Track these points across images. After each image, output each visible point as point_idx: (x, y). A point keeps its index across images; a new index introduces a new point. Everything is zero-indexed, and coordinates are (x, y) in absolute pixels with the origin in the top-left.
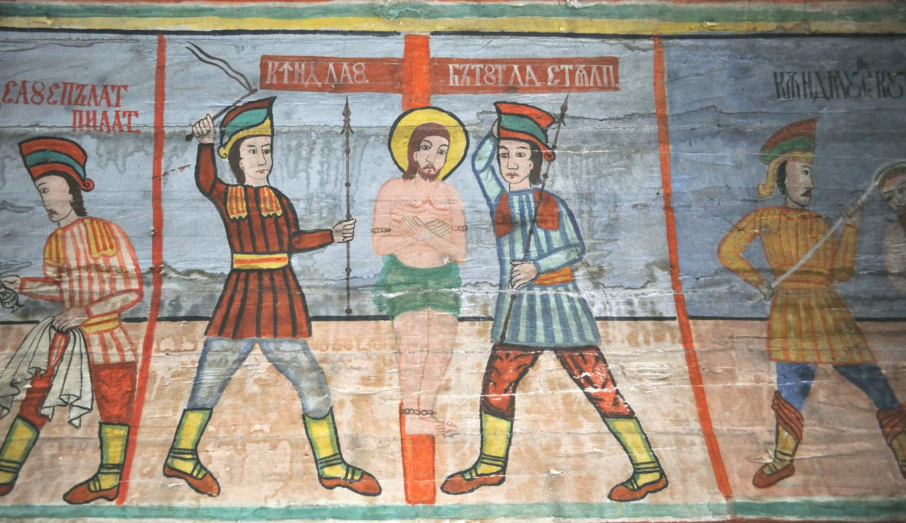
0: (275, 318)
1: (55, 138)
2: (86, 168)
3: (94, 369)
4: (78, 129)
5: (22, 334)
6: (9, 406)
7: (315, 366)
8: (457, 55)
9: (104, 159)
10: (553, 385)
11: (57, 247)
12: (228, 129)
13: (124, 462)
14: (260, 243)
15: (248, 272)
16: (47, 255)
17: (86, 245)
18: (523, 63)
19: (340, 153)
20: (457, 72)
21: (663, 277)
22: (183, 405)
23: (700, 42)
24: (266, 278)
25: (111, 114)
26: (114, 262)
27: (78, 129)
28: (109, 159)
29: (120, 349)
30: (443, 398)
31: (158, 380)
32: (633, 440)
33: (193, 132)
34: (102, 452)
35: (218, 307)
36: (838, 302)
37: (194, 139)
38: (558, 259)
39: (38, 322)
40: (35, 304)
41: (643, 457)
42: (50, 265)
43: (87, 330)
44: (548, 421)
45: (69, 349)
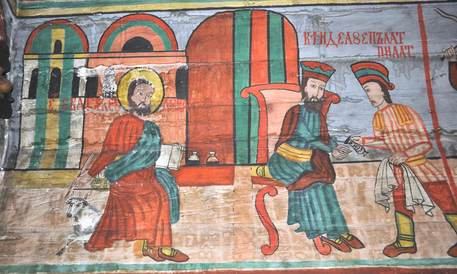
1: (370, 62)
2: (389, 77)
3: (427, 186)
4: (381, 57)
6: (388, 206)
9: (398, 72)
11: (380, 120)
16: (375, 125)
17: (396, 119)
26: (412, 127)
27: (381, 57)
28: (400, 72)
29: (434, 174)
34: (454, 229)
39: (381, 161)
40: (375, 151)
43: (410, 164)
45: (405, 174)
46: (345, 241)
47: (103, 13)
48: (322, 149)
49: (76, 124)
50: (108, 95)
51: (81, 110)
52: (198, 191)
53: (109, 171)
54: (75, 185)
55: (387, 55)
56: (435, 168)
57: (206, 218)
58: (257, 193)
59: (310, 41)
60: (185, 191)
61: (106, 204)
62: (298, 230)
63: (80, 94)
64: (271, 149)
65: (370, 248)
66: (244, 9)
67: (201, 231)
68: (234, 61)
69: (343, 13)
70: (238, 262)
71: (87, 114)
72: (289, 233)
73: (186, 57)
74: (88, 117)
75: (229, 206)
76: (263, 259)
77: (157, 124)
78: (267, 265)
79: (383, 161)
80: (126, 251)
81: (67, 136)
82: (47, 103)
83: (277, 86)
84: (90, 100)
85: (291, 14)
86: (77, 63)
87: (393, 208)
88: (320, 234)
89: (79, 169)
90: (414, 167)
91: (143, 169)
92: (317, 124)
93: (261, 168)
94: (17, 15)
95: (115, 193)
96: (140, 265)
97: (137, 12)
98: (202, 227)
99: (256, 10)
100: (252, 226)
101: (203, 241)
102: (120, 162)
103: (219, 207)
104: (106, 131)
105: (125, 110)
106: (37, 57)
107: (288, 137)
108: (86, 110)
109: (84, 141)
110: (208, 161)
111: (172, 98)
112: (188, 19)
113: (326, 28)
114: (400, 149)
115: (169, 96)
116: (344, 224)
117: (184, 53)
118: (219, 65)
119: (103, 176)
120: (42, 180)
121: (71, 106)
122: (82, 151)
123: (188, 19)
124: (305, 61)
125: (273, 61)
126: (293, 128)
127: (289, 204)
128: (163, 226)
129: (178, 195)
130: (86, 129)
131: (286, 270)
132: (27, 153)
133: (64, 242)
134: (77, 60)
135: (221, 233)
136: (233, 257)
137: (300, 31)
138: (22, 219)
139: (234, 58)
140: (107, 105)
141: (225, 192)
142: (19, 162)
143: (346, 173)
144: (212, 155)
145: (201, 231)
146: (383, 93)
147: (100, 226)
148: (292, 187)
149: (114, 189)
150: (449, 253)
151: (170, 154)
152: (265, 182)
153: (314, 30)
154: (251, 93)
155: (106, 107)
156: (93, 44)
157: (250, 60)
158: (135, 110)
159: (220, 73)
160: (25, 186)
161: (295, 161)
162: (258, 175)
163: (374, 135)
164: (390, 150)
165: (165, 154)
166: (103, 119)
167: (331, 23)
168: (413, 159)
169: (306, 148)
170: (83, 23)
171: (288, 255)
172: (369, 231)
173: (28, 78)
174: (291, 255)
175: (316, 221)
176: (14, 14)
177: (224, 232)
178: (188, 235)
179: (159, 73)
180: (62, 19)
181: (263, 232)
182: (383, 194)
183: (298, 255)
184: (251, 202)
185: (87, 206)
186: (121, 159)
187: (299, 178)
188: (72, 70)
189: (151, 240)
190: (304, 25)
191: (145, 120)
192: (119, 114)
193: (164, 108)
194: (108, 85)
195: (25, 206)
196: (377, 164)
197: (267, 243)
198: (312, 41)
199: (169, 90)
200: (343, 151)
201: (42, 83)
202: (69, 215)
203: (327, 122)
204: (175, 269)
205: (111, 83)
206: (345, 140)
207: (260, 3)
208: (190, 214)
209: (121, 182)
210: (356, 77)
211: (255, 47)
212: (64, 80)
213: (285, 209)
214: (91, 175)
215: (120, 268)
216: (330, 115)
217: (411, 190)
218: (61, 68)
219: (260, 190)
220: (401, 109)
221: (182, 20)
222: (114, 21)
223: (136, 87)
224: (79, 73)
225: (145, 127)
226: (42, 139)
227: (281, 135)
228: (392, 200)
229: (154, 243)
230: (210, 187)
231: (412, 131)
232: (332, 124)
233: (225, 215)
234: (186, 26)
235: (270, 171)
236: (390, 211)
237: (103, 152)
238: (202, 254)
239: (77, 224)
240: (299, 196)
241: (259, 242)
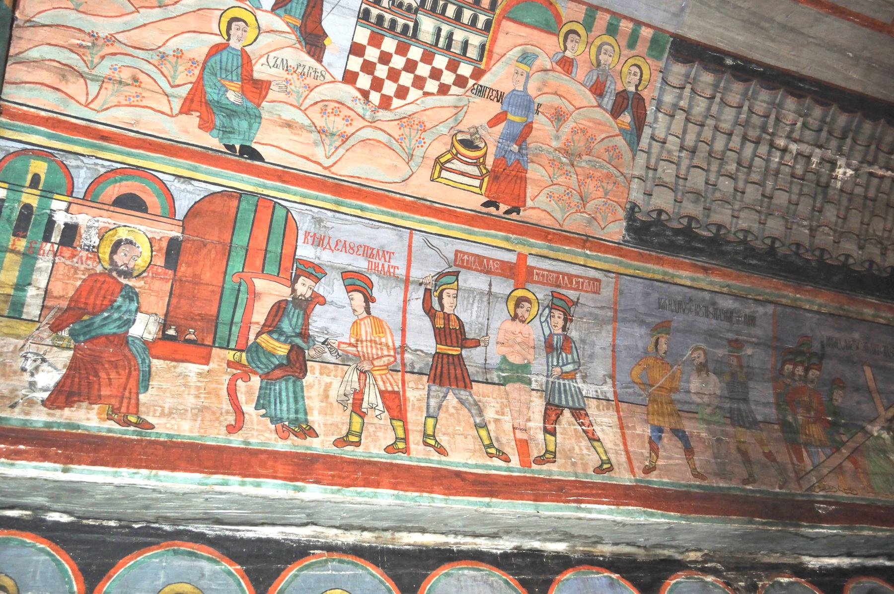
0: (456, 378)
3: (381, 392)
7: (476, 403)
8: (538, 266)
10: (570, 424)
12: (438, 283)
14: (449, 341)
15: (443, 354)
18: (564, 274)
19: (486, 303)
20: (537, 274)
21: (609, 381)
22: (425, 415)
23: (633, 279)
24: (451, 358)
26: (383, 340)
29: (391, 385)
30: (529, 424)
32: (600, 450)
35: (431, 369)
36: (672, 402)
38: (569, 368)
40: (347, 356)
41: (604, 458)
43: (374, 373)
44: (569, 439)
46: (303, 430)
47: (97, 158)
51: (51, 257)
53: (74, 329)
62: (263, 416)
63: (53, 240)
64: (252, 337)
66: (252, 194)
68: (231, 242)
77: (137, 290)
78: (230, 441)
82: (9, 241)
83: (269, 277)
84: (64, 248)
86: (55, 205)
87: (350, 408)
89: (38, 322)
91: (115, 334)
92: (300, 321)
93: (239, 353)
96: (103, 428)
100: (220, 406)
101: (171, 413)
106: (6, 186)
108: (57, 258)
117: (181, 223)
126: (277, 320)
129: (149, 367)
133: (17, 396)
139: (232, 240)
140: (84, 259)
143: (317, 371)
147: (59, 387)
148: (265, 377)
158: (116, 270)
166: (76, 273)
169: (285, 342)
170: (71, 162)
172: (325, 425)
174: (253, 435)
175: (281, 410)
177: (192, 409)
182: (345, 395)
184: (223, 384)
186: (90, 319)
187: (273, 370)
188: (48, 211)
189: (117, 406)
190: (306, 225)
196: (346, 368)
197: (233, 423)
198: (310, 241)
212: (36, 220)
227: (264, 325)
228: (351, 401)
229: (119, 409)
232: (313, 324)
234: (189, 196)
237: (69, 308)
239: (32, 379)
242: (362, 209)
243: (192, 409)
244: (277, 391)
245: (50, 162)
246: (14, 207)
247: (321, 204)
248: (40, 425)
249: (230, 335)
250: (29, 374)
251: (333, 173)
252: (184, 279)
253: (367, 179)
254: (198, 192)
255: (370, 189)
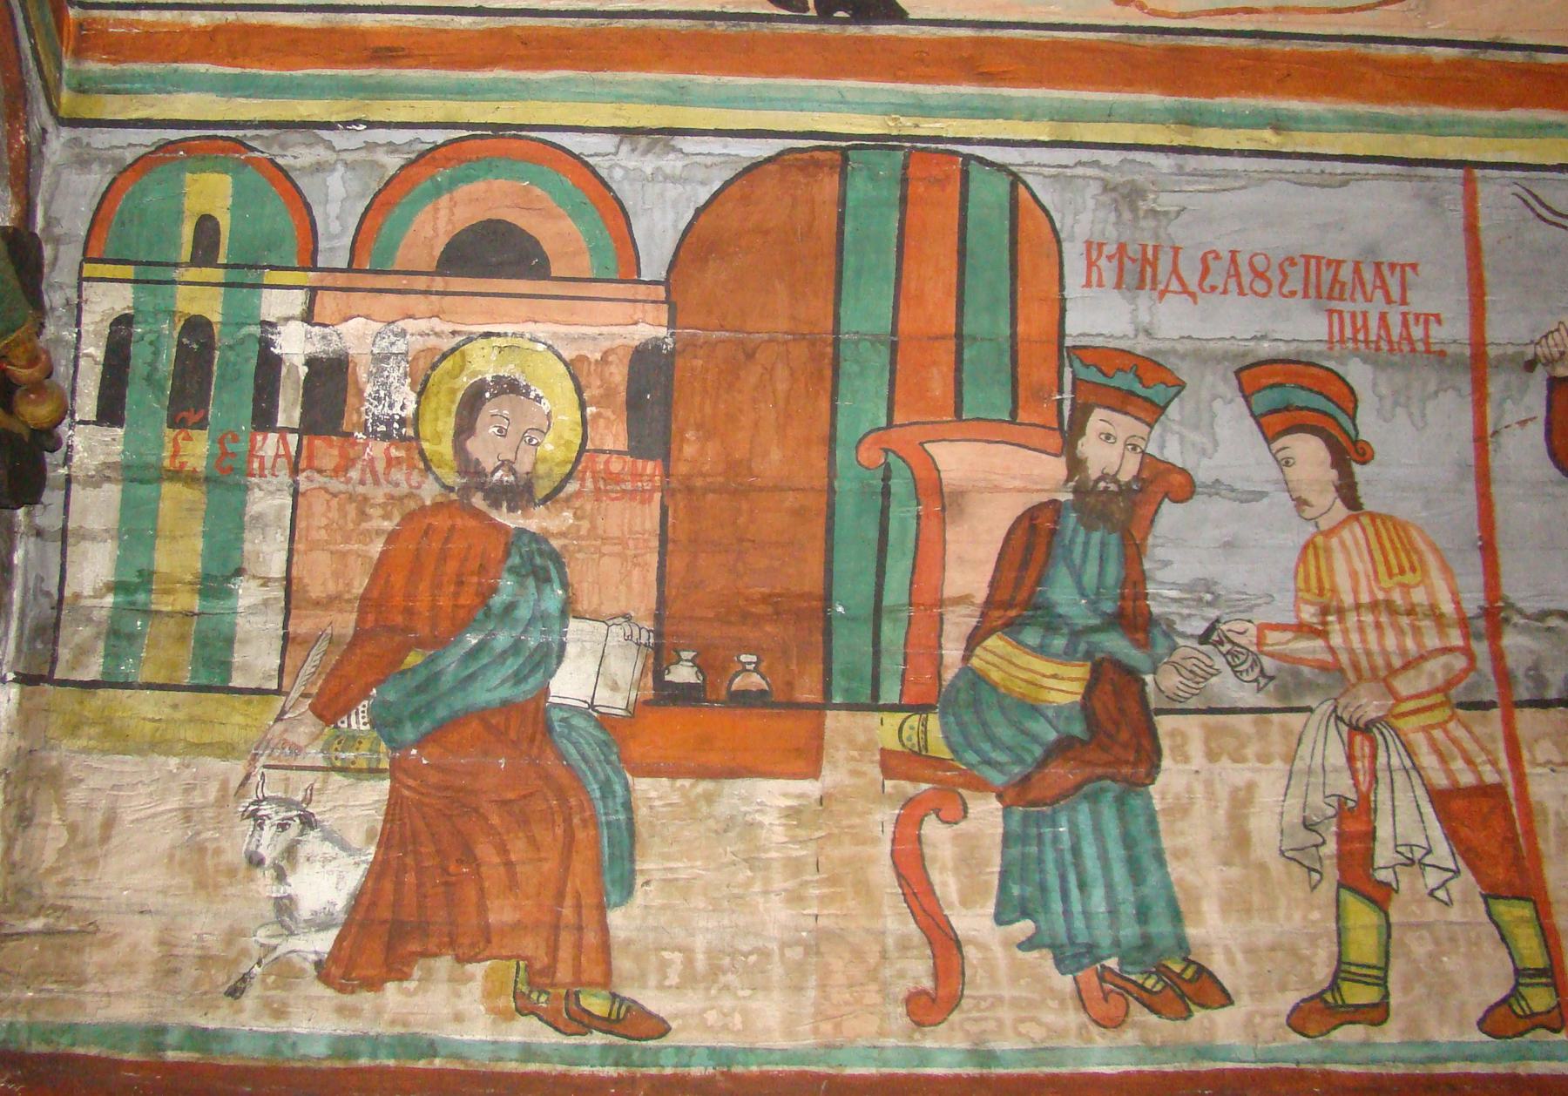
1: (1299, 362)
2: (1358, 422)
3: (1441, 799)
4: (1337, 347)
5: (1291, 732)
6: (1317, 867)
9: (1388, 404)
11: (1318, 569)
13: (1551, 965)
16: (1301, 584)
17: (1370, 566)
25: (1395, 320)
26: (1419, 596)
27: (1337, 347)
28: (1396, 404)
29: (1469, 761)
31: (1551, 817)
33: (1536, 355)
34: (1508, 947)
37: (1539, 368)
39: (1309, 710)
40: (1296, 674)
42: (1307, 602)
43: (1401, 724)
45: (1382, 759)
47: (371, 125)
48: (1125, 660)
49: (266, 525)
50: (382, 428)
51: (284, 477)
52: (698, 796)
53: (386, 705)
54: (267, 752)
55: (1355, 340)
56: (1477, 740)
57: (725, 891)
58: (897, 812)
59: (1104, 274)
60: (653, 794)
61: (379, 828)
62: (1029, 944)
63: (281, 421)
64: (952, 652)
65: (1249, 1008)
66: (881, 142)
67: (709, 936)
69: (1220, 183)
70: (828, 1047)
71: (304, 494)
72: (998, 952)
73: (665, 307)
74: (310, 506)
75: (803, 853)
76: (910, 1038)
77: (556, 543)
78: (925, 1057)
79: (1317, 711)
80: (458, 995)
81: (232, 568)
82: (162, 446)
84: (318, 442)
85: (1046, 171)
86: (279, 303)
87: (1332, 873)
88: (1099, 959)
89: (278, 692)
90: (1412, 736)
91: (506, 705)
93: (915, 720)
94: (62, 113)
95: (409, 788)
96: (507, 1045)
97: (498, 128)
98: (712, 924)
99: (923, 149)
101: (715, 971)
102: (422, 675)
103: (768, 856)
104: (371, 558)
105: (445, 486)
106: (129, 271)
107: (1013, 613)
108: (301, 478)
109: (294, 588)
110: (734, 688)
111: (611, 452)
112: (679, 164)
113: (1162, 233)
114: (1373, 669)
115: (603, 444)
116: (1174, 926)
117: (661, 292)
118: (786, 342)
119: (365, 724)
120: (149, 726)
121: (250, 462)
122: (285, 626)
123: (679, 164)
124: (1085, 347)
125: (974, 339)
127: (1003, 854)
128: (579, 914)
129: (628, 807)
130: (300, 546)
131: (982, 1076)
132: (89, 620)
133: (245, 952)
134: (275, 291)
135: (774, 946)
136: (816, 1031)
137: (1072, 238)
138: (91, 863)
140: (380, 466)
141: (790, 802)
142: (64, 654)
143: (1196, 749)
144: (748, 667)
145: (709, 936)
146: (1333, 474)
148: (1018, 794)
149: (406, 771)
150: (1481, 1024)
151: (600, 654)
152: (928, 772)
153: (1119, 235)
154: (894, 452)
155: (374, 473)
156: (332, 237)
157: (894, 332)
158: (481, 487)
159: (786, 373)
160: (92, 743)
161: (1030, 701)
162: (903, 745)
163: (1297, 616)
164: (1342, 670)
165: (581, 654)
166: (363, 515)
167: (1178, 213)
168: (1411, 705)
169: (1068, 655)
170: (298, 156)
171: (991, 1025)
172: (1250, 951)
173: (97, 347)
174: (1000, 1023)
175: (1087, 914)
176: (53, 111)
177: (784, 945)
178: (665, 949)
179: (568, 359)
180: (228, 138)
181: (913, 948)
183: (1023, 1028)
184: (875, 841)
185: (313, 829)
186: (425, 664)
187: (1042, 764)
189: (542, 960)
190: (1086, 218)
191: (512, 526)
192: (422, 500)
193: (582, 486)
194: (382, 393)
195: (98, 818)
196: (1296, 720)
197: (927, 983)
198: (1109, 276)
199: (602, 422)
200: (1191, 672)
201: (145, 370)
202: (255, 859)
203: (1147, 565)
204: (623, 1061)
205: (396, 384)
206: (1200, 631)
207: (938, 125)
208: (670, 876)
209: (432, 748)
210: (1253, 414)
211: (913, 285)
212: (225, 363)
213: (988, 870)
214: (320, 716)
215: (442, 1051)
216: (1160, 541)
217: (1394, 815)
218: (216, 318)
219: (910, 803)
220: (1388, 530)
221: (658, 169)
222: (413, 156)
223: (484, 404)
224: (278, 340)
225: (514, 551)
226: (140, 573)
227: (989, 603)
228: (1331, 847)
229: (550, 970)
230: (739, 781)
231: (1418, 609)
233: (790, 884)
234: (673, 191)
235: (943, 732)
236: (1324, 886)
237: (360, 636)
238: (712, 1017)
239: (282, 891)
240: (1038, 826)
241: (901, 982)
242: (1279, 124)
243: (784, 945)
244: (1066, 843)
245: (237, 169)
246: (160, 335)
247: (1126, 133)
248: (320, 1049)
249: (877, 654)
250: (270, 873)
251: (1154, 13)
252: (699, 483)
253: (1278, 10)
254: (700, 174)
255: (1296, 45)
